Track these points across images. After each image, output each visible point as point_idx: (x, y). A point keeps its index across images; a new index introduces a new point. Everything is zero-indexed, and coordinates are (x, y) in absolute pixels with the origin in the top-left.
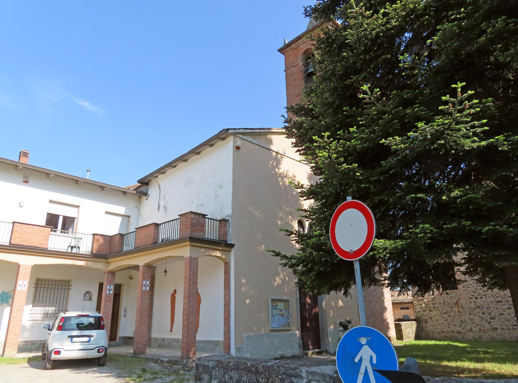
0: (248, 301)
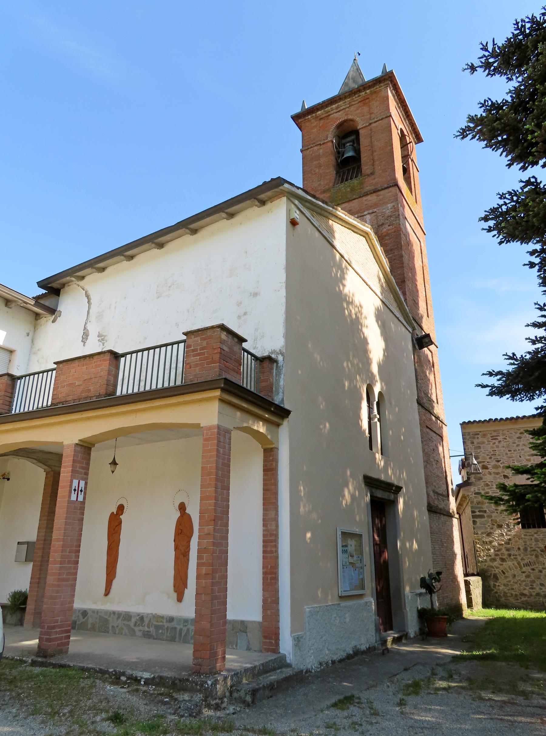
0: (309, 535)
